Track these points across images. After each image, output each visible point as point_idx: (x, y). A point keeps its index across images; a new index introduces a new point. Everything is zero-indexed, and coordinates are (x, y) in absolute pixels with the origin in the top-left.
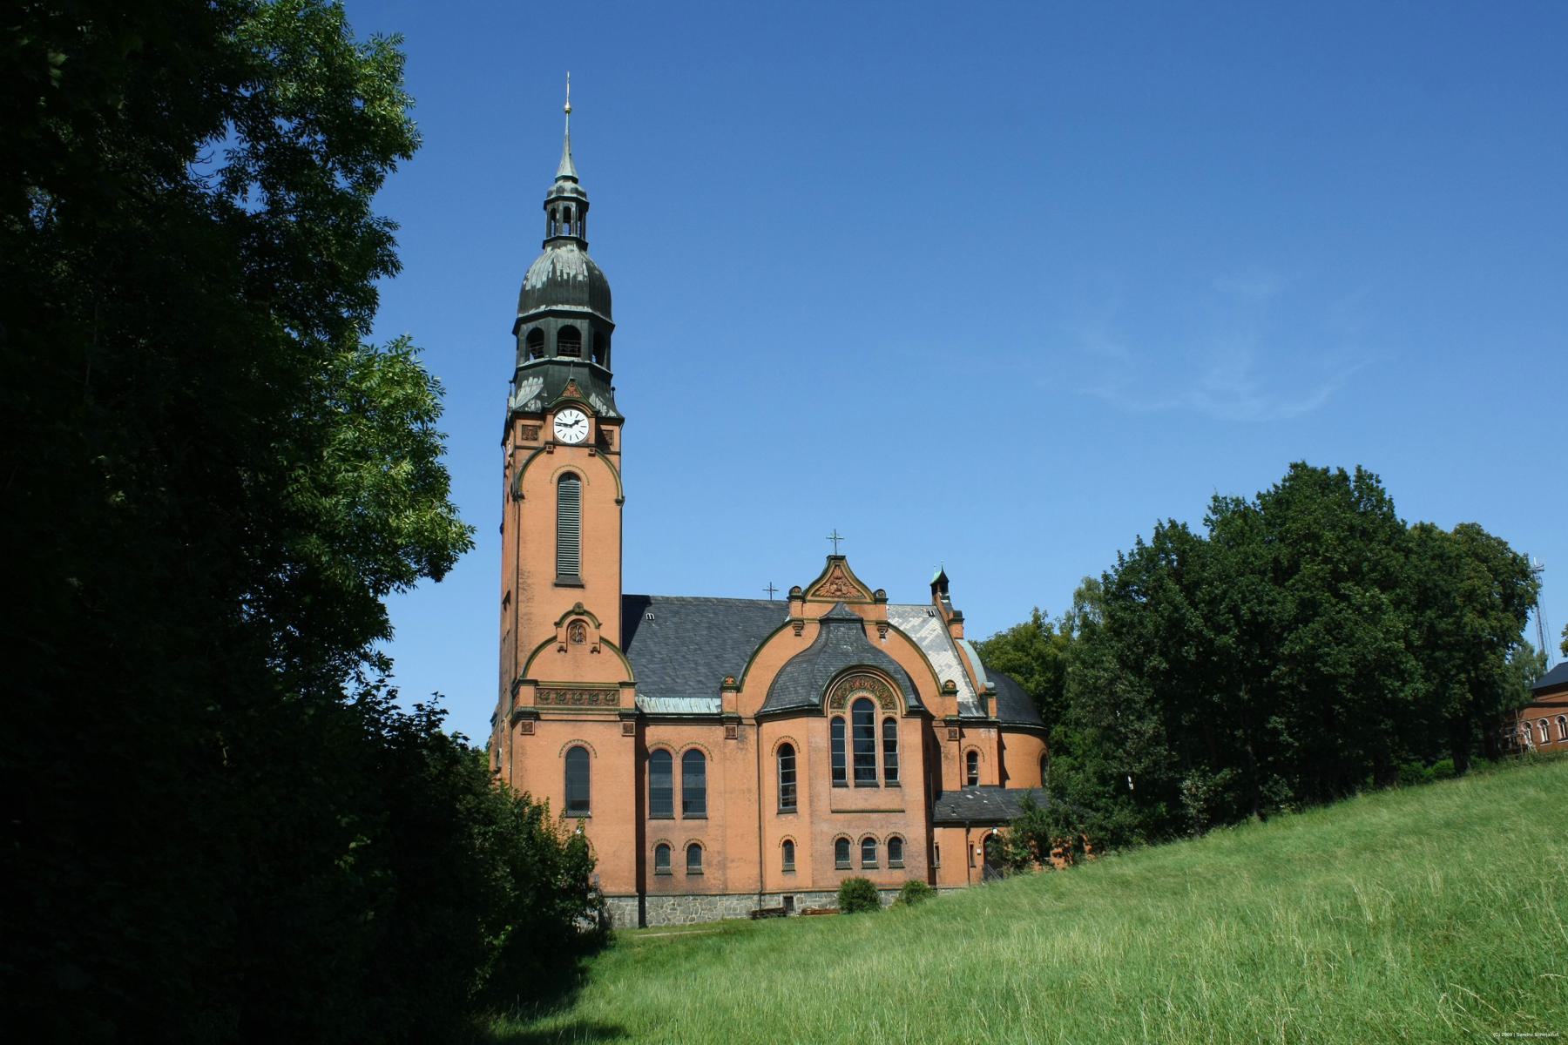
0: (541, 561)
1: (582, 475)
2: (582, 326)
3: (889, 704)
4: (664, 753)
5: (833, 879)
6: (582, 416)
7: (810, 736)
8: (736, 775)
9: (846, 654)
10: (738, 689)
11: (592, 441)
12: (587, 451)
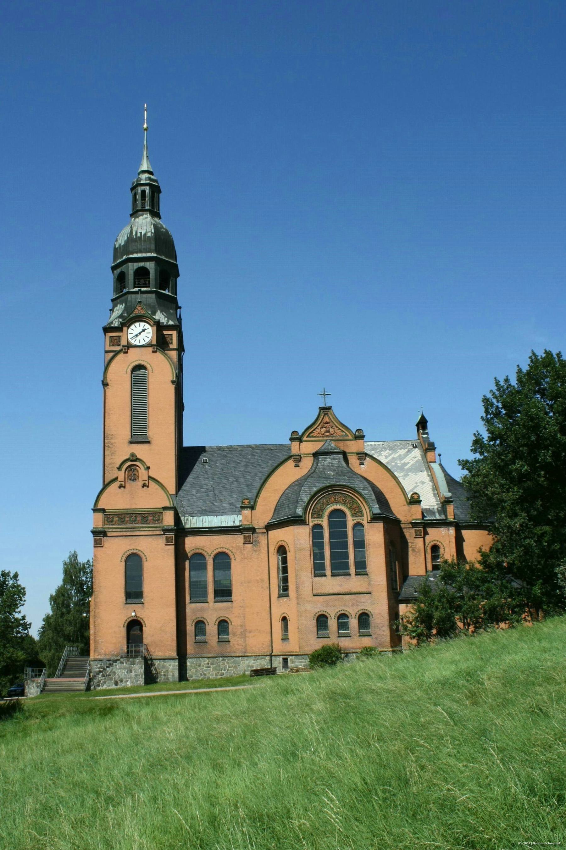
0: (121, 427)
1: (148, 366)
2: (151, 266)
3: (357, 512)
4: (199, 556)
5: (314, 644)
6: (147, 326)
7: (298, 538)
8: (251, 569)
9: (327, 478)
10: (252, 508)
11: (154, 342)
12: (151, 349)
